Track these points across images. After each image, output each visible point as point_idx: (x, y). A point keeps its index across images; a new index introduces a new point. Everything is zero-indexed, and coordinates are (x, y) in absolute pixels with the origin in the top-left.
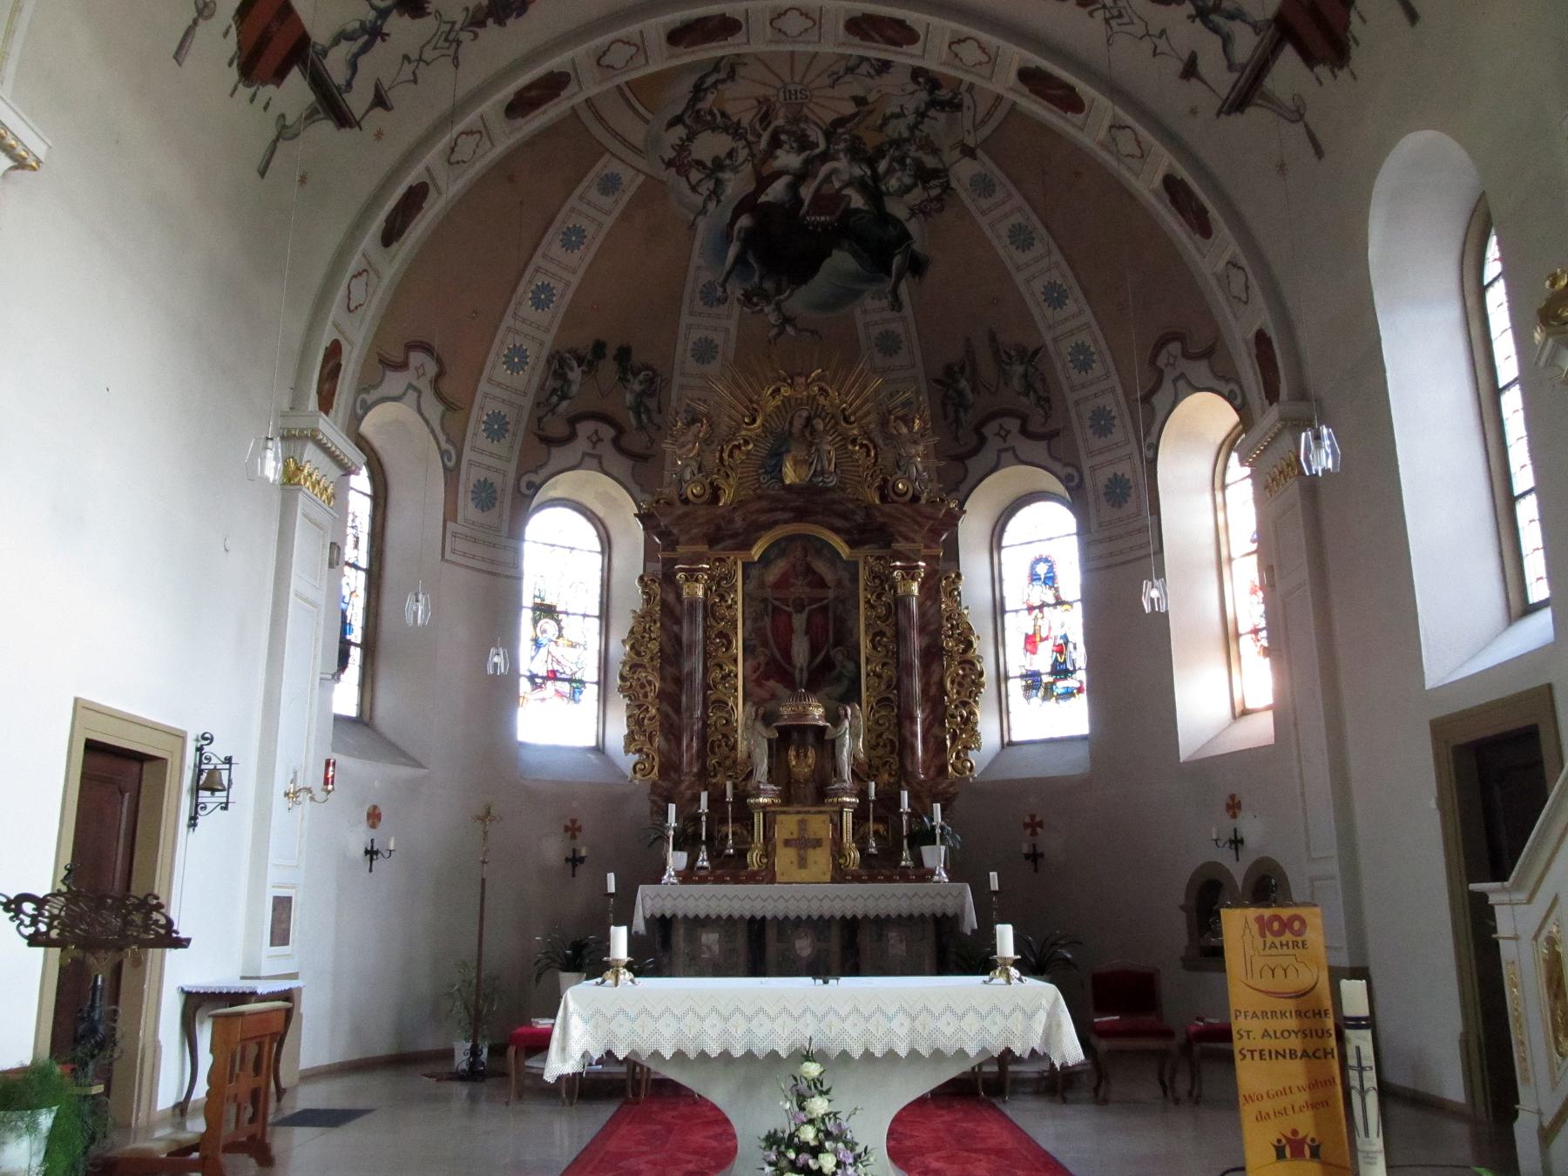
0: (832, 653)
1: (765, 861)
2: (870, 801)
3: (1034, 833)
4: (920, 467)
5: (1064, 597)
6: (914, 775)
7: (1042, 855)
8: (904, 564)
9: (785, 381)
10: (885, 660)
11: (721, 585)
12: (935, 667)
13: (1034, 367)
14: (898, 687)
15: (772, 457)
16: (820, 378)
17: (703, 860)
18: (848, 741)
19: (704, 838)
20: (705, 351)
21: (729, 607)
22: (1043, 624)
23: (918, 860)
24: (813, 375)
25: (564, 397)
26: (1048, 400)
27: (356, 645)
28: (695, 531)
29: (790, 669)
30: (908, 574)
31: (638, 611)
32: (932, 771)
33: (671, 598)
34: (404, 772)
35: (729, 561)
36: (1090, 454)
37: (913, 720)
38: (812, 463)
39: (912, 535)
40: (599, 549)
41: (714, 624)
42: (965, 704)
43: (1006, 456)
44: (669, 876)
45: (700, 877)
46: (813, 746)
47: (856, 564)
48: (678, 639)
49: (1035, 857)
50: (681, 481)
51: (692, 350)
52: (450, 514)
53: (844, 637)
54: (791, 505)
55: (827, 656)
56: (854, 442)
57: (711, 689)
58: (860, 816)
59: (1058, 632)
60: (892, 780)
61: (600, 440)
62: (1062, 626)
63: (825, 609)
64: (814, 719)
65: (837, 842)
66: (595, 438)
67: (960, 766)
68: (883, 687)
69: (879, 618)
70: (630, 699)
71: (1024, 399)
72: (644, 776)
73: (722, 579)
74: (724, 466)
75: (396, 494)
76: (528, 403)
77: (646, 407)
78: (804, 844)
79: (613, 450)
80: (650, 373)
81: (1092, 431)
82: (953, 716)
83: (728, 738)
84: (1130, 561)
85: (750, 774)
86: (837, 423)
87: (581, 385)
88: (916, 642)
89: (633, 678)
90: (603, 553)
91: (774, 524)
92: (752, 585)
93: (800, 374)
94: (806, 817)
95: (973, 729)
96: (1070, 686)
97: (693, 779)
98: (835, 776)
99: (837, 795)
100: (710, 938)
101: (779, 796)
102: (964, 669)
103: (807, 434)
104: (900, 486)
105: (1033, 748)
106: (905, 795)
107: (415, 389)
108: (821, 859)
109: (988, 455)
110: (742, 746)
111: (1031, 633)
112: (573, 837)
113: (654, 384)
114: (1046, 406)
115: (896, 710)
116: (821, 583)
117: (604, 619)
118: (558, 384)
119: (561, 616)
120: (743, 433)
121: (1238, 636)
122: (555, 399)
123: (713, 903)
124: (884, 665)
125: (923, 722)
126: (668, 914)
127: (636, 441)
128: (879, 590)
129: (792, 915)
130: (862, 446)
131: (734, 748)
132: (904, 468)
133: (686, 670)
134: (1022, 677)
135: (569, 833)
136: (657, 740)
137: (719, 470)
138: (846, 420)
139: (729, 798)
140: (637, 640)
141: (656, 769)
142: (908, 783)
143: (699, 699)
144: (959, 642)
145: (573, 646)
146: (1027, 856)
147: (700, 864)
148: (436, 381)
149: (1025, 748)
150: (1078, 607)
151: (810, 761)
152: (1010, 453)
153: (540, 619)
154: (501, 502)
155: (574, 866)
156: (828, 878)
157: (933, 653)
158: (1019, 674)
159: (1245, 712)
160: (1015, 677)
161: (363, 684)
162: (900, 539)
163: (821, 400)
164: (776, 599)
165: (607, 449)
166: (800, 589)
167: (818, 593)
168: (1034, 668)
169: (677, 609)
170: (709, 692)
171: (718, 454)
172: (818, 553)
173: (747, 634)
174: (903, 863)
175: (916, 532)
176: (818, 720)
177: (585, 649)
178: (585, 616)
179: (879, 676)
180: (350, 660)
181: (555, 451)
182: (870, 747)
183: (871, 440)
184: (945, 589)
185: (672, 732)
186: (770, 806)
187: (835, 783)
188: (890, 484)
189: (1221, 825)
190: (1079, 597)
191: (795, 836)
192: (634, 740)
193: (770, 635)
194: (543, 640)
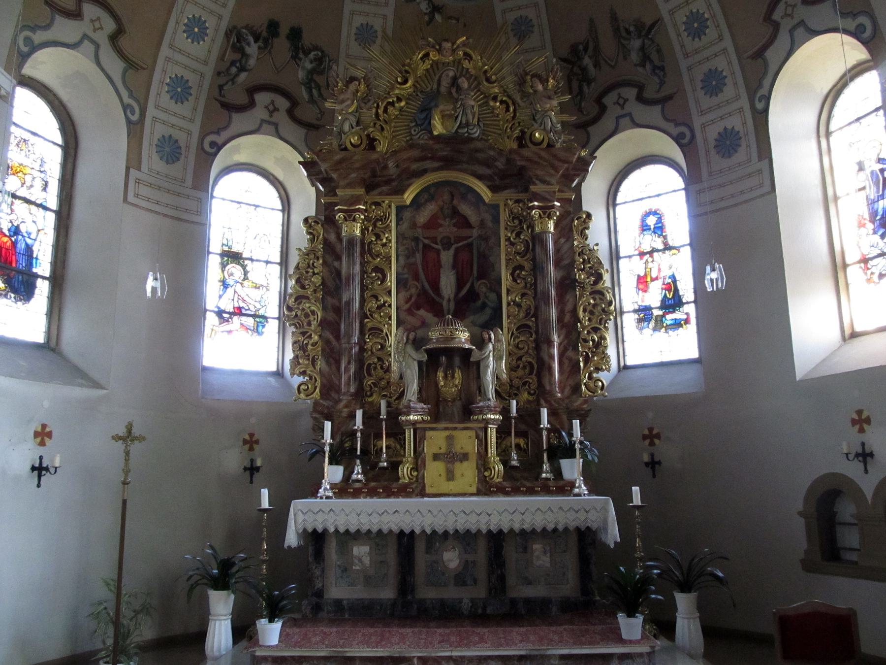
0: (477, 285)
1: (415, 474)
2: (511, 418)
3: (652, 444)
4: (554, 120)
5: (671, 243)
6: (551, 393)
7: (659, 463)
8: (541, 204)
9: (433, 47)
10: (526, 291)
11: (376, 226)
12: (569, 297)
13: (651, 39)
14: (535, 315)
15: (422, 111)
16: (464, 44)
17: (358, 473)
18: (491, 363)
19: (359, 453)
20: (366, 35)
21: (384, 245)
22: (654, 267)
23: (558, 472)
24: (458, 42)
25: (242, 69)
26: (662, 69)
27: (44, 278)
28: (353, 175)
29: (437, 299)
30: (544, 213)
31: (303, 249)
32: (567, 391)
33: (332, 237)
34: (78, 392)
35: (384, 205)
36: (702, 113)
37: (550, 343)
38: (457, 117)
39: (548, 179)
40: (280, 208)
41: (370, 259)
42: (596, 330)
43: (625, 121)
44: (325, 489)
45: (355, 489)
46: (459, 368)
47: (497, 206)
48: (338, 273)
49: (653, 464)
50: (341, 132)
51: (356, 34)
52: (133, 161)
53: (487, 271)
54: (441, 154)
55: (472, 289)
56: (495, 99)
57: (368, 318)
58: (503, 432)
59: (666, 273)
60: (531, 398)
61: (276, 109)
62: (671, 268)
63: (470, 245)
64: (460, 342)
65: (483, 456)
66: (271, 108)
67: (591, 385)
68: (522, 315)
69: (519, 254)
70: (296, 327)
71: (640, 69)
72: (307, 396)
73: (377, 220)
74: (379, 120)
75: (85, 143)
76: (209, 71)
77: (316, 82)
78: (451, 458)
79: (289, 121)
80: (320, 54)
81: (703, 92)
82: (586, 341)
83: (383, 361)
84: (741, 203)
85: (402, 394)
86: (479, 84)
87: (258, 59)
88: (553, 273)
89: (298, 308)
90: (283, 211)
91: (424, 172)
92: (405, 226)
93: (446, 40)
94: (454, 433)
95: (603, 352)
96: (678, 318)
97: (350, 398)
98: (480, 395)
99: (481, 412)
100: (361, 551)
101: (429, 413)
102: (594, 299)
103: (454, 94)
104: (537, 135)
105: (646, 370)
106: (544, 412)
107: (92, 41)
108: (467, 473)
109: (608, 122)
110: (395, 367)
111: (642, 274)
112: (251, 449)
113: (322, 64)
114: (662, 73)
115: (534, 336)
116: (465, 223)
117: (284, 266)
118: (237, 56)
119: (246, 262)
120: (397, 91)
121: (845, 266)
122: (234, 70)
123: (364, 519)
124: (523, 295)
125: (560, 344)
126: (320, 529)
127: (308, 113)
128: (518, 229)
129: (440, 530)
130: (502, 102)
131: (388, 370)
132: (539, 121)
133: (345, 299)
134: (635, 311)
135: (248, 446)
136: (320, 364)
137: (375, 124)
138: (488, 80)
139: (383, 416)
140: (301, 274)
141: (318, 390)
142: (546, 401)
143: (357, 326)
144: (589, 275)
145: (257, 287)
146: (647, 464)
147: (354, 477)
148: (114, 38)
149: (639, 372)
150: (687, 252)
151: (457, 382)
152: (627, 119)
153: (228, 264)
154: (187, 157)
155: (252, 475)
156: (474, 490)
157: (567, 285)
158: (632, 309)
159: (854, 335)
160: (629, 312)
161: (50, 314)
162: (537, 182)
163: (466, 64)
164: (425, 238)
165: (282, 117)
166: (447, 229)
167: (465, 232)
168: (646, 303)
169: (338, 247)
170: (366, 320)
171: (374, 110)
172: (463, 197)
173: (400, 270)
174: (544, 475)
175: (551, 175)
176: (464, 343)
177: (268, 290)
178: (267, 262)
179: (519, 305)
180: (37, 291)
181: (236, 117)
182: (512, 369)
183: (509, 97)
184: (577, 227)
185: (332, 356)
186: (420, 423)
187: (480, 401)
188: (528, 135)
189: (850, 441)
190: (688, 241)
191: (443, 450)
192: (299, 363)
193: (420, 267)
194: (230, 281)
